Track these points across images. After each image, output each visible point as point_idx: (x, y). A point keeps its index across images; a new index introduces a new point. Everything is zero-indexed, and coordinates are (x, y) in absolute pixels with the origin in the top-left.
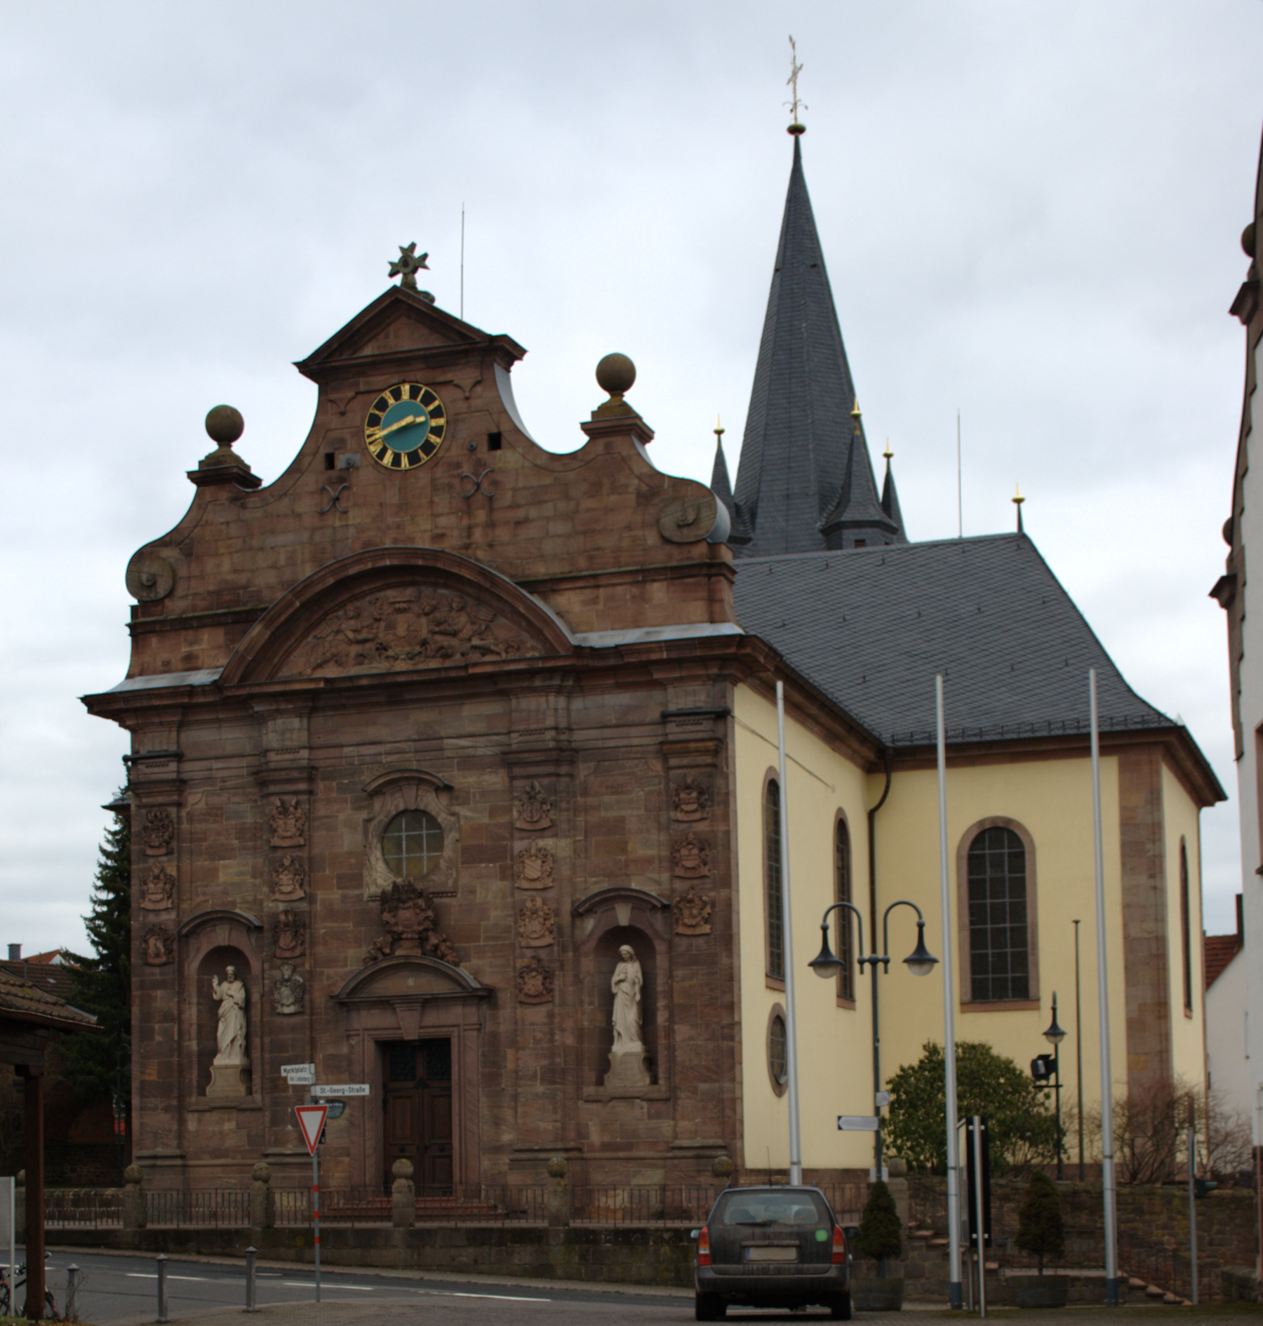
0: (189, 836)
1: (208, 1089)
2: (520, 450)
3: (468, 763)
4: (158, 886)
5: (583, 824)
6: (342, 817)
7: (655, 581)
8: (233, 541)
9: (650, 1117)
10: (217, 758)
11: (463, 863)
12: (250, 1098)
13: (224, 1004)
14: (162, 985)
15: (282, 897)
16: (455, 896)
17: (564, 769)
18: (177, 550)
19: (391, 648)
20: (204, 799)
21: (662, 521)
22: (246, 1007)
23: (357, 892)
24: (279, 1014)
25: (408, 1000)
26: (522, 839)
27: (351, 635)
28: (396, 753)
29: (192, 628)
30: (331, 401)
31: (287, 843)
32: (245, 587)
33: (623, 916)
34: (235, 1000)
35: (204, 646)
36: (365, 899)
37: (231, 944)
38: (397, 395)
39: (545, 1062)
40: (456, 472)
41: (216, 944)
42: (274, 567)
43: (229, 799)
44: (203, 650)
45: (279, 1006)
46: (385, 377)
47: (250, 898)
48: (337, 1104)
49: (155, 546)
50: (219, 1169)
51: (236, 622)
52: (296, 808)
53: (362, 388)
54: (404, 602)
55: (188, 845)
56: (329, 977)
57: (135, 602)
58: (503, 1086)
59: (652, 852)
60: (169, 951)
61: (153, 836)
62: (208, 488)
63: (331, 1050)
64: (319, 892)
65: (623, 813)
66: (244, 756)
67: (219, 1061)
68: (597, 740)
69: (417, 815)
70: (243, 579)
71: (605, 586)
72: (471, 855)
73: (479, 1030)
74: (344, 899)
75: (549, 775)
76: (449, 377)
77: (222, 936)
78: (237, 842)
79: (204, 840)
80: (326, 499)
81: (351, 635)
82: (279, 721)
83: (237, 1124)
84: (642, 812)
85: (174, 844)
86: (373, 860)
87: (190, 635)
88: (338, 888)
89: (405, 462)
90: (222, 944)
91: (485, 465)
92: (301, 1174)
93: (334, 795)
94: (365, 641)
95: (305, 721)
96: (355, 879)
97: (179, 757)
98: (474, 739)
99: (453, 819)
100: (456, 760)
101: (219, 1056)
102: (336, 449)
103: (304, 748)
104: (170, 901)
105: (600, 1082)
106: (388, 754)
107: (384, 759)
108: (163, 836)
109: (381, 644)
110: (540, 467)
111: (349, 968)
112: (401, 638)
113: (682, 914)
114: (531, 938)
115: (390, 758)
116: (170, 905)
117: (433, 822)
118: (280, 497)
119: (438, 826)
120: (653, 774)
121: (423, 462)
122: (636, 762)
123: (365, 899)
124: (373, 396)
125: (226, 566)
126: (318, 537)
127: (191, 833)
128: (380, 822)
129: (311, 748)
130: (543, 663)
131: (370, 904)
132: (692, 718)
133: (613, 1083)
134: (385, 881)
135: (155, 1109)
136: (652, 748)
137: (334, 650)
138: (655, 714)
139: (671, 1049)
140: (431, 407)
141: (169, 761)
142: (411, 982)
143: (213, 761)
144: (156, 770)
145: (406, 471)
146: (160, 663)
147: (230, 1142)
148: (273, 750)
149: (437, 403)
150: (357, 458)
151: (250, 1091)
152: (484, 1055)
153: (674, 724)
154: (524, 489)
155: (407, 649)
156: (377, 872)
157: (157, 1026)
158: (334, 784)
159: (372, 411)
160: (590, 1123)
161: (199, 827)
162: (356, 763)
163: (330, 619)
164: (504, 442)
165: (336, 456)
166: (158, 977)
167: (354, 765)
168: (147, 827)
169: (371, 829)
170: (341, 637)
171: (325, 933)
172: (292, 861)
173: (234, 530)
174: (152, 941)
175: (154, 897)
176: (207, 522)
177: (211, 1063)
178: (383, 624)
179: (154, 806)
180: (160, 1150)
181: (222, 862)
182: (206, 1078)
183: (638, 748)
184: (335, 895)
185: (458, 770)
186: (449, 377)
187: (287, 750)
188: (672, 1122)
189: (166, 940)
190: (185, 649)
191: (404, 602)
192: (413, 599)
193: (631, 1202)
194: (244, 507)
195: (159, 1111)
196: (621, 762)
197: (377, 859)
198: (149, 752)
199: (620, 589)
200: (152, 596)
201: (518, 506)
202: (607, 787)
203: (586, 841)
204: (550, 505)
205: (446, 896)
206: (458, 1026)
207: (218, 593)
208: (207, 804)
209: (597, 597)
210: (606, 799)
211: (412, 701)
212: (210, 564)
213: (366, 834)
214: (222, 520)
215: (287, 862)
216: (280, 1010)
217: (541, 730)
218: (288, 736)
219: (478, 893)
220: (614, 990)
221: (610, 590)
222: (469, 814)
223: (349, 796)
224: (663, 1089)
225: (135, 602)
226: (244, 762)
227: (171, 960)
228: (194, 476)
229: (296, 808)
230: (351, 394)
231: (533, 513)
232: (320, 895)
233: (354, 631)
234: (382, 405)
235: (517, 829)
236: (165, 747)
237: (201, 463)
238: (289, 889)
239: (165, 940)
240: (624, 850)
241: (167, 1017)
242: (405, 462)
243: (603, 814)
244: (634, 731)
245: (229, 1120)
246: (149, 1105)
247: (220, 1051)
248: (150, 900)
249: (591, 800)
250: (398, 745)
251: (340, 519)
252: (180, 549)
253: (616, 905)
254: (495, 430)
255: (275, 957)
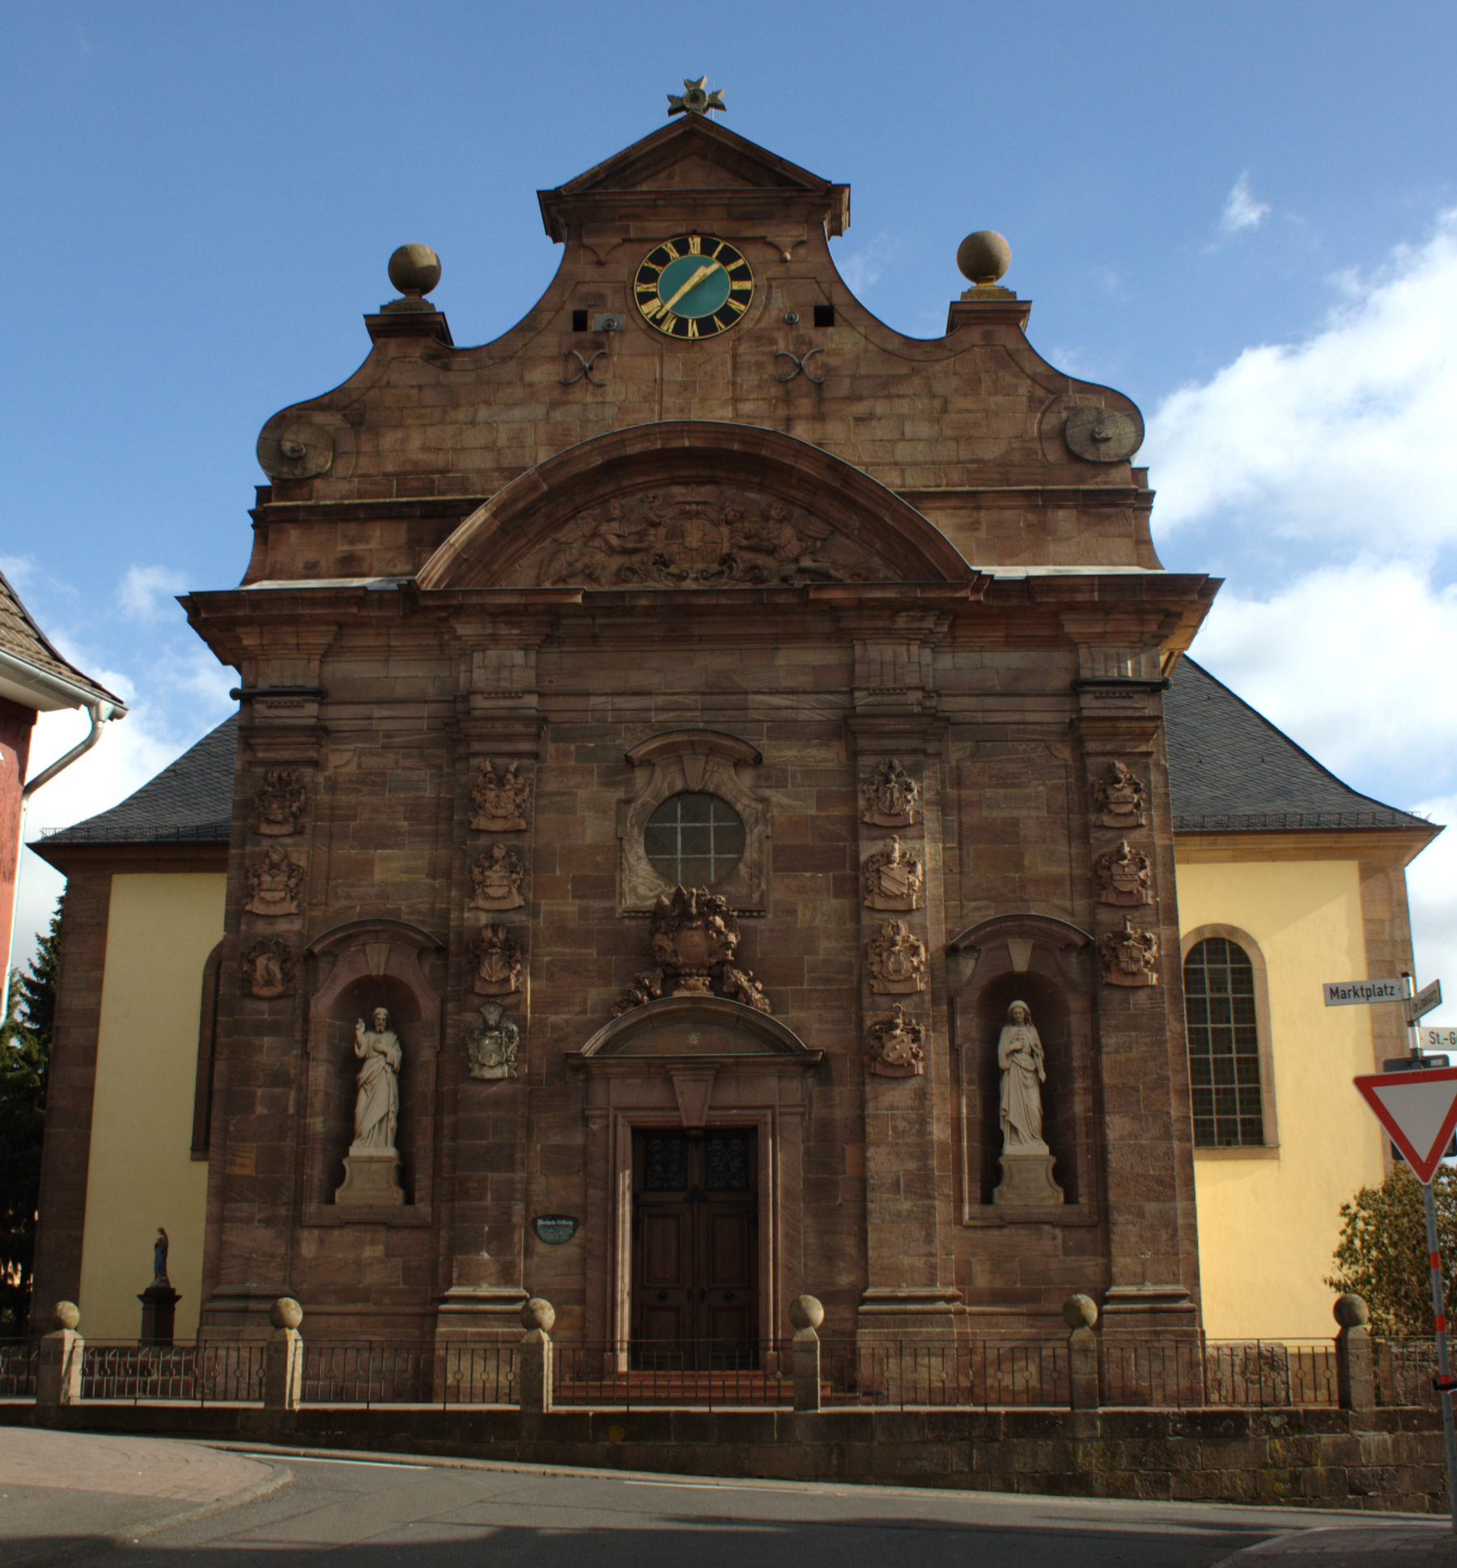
0: (328, 812)
1: (338, 1193)
2: (862, 330)
3: (785, 730)
4: (277, 879)
5: (956, 825)
6: (583, 794)
7: (1060, 507)
8: (426, 410)
9: (1067, 1251)
10: (381, 702)
11: (775, 870)
12: (409, 1209)
13: (367, 1065)
14: (273, 1029)
15: (487, 905)
16: (763, 917)
17: (932, 748)
18: (340, 416)
19: (673, 562)
20: (356, 759)
21: (1069, 432)
22: (404, 1073)
23: (605, 904)
24: (475, 1079)
25: (695, 1065)
26: (873, 839)
27: (614, 541)
28: (672, 710)
29: (357, 519)
30: (585, 247)
31: (498, 825)
32: (443, 472)
33: (1020, 958)
34: (389, 1059)
35: (373, 545)
36: (618, 916)
37: (389, 973)
38: (683, 248)
39: (912, 1165)
40: (767, 349)
41: (365, 973)
42: (490, 447)
43: (397, 762)
44: (371, 550)
45: (476, 1067)
46: (667, 224)
47: (424, 907)
48: (564, 1222)
49: (302, 409)
50: (353, 1319)
51: (424, 517)
52: (516, 776)
53: (632, 234)
54: (697, 503)
55: (326, 824)
56: (555, 1027)
57: (265, 481)
58: (840, 1201)
59: (1062, 870)
60: (288, 977)
61: (275, 806)
62: (392, 340)
63: (556, 1139)
64: (543, 902)
65: (1015, 813)
66: (426, 702)
67: (355, 1150)
68: (978, 711)
69: (695, 800)
70: (437, 460)
71: (988, 509)
72: (789, 859)
73: (802, 1115)
74: (584, 913)
75: (914, 752)
76: (760, 232)
77: (376, 960)
78: (406, 823)
79: (354, 818)
80: (572, 367)
81: (614, 541)
82: (492, 654)
83: (387, 1249)
84: (1044, 813)
85: (307, 821)
86: (632, 859)
87: (353, 529)
88: (574, 897)
89: (693, 330)
90: (374, 973)
91: (810, 344)
92: (506, 1330)
93: (572, 763)
94: (635, 551)
95: (533, 657)
96: (606, 884)
97: (320, 695)
98: (795, 697)
99: (760, 806)
100: (765, 725)
101: (356, 1143)
102: (591, 306)
103: (530, 692)
104: (295, 903)
105: (987, 1198)
106: (658, 709)
107: (654, 717)
108: (291, 806)
109: (661, 556)
110: (891, 353)
111: (589, 1016)
112: (691, 550)
113: (1117, 957)
114: (890, 980)
115: (663, 717)
116: (293, 910)
117: (727, 807)
118: (503, 360)
119: (738, 816)
120: (1059, 763)
121: (720, 332)
122: (1033, 745)
123: (618, 916)
124: (647, 246)
125: (416, 441)
126: (558, 415)
127: (332, 808)
128: (644, 805)
129: (541, 695)
130: (922, 592)
131: (626, 921)
132: (1118, 689)
133: (1007, 1197)
134: (650, 890)
135: (248, 1220)
136: (1054, 728)
137: (586, 560)
138: (1061, 681)
139: (1100, 1153)
140: (733, 267)
141: (306, 701)
142: (694, 1039)
143: (374, 707)
144: (284, 712)
145: (693, 341)
146: (301, 565)
147: (372, 1278)
148: (482, 693)
149: (741, 262)
150: (620, 321)
151: (409, 1200)
152: (807, 1152)
153: (1090, 696)
154: (868, 377)
155: (700, 566)
156: (637, 875)
157: (259, 1092)
158: (572, 747)
159: (646, 264)
160: (973, 1260)
161: (343, 799)
162: (610, 720)
163: (583, 518)
164: (837, 317)
165: (589, 314)
166: (266, 1016)
167: (605, 721)
168: (265, 793)
169: (630, 814)
170: (597, 543)
171: (550, 962)
172: (508, 853)
173: (429, 396)
174: (261, 962)
175: (268, 896)
176: (388, 383)
177: (346, 1154)
178: (662, 531)
179: (276, 763)
180: (253, 1286)
181: (379, 851)
182: (337, 1175)
183: (1035, 727)
184: (570, 907)
185: (769, 738)
186: (760, 232)
187: (503, 693)
188: (1101, 1260)
189: (285, 958)
190: (342, 548)
191: (697, 503)
192: (711, 500)
193: (1041, 1381)
194: (446, 368)
195: (256, 1224)
196: (1010, 744)
197: (639, 858)
198: (272, 687)
199: (1009, 515)
200: (298, 472)
201: (860, 399)
202: (991, 777)
203: (960, 849)
204: (905, 402)
205: (751, 917)
206: (772, 1107)
207: (400, 475)
208: (359, 767)
209: (978, 522)
210: (989, 792)
211: (701, 639)
212: (389, 440)
213: (620, 819)
214: (413, 383)
215: (498, 853)
216: (476, 1073)
217: (901, 689)
218: (505, 674)
219: (800, 913)
220: (1003, 1063)
221: (995, 515)
222: (785, 801)
223: (595, 765)
224: (1086, 1210)
225: (265, 481)
226: (425, 711)
227: (292, 992)
228: (375, 321)
229: (516, 776)
230: (616, 240)
231: (881, 407)
232: (545, 906)
233: (618, 536)
234: (661, 258)
235: (866, 823)
236: (300, 682)
237: (383, 308)
238: (500, 892)
239: (284, 961)
240: (1018, 865)
241: (279, 1078)
242: (693, 330)
243: (985, 813)
244: (1029, 702)
245: (373, 1243)
246: (239, 1214)
247: (360, 1136)
248: (262, 899)
249: (966, 793)
250: (676, 698)
251: (594, 394)
252: (344, 416)
253: (1010, 941)
254: (825, 303)
255: (472, 992)
